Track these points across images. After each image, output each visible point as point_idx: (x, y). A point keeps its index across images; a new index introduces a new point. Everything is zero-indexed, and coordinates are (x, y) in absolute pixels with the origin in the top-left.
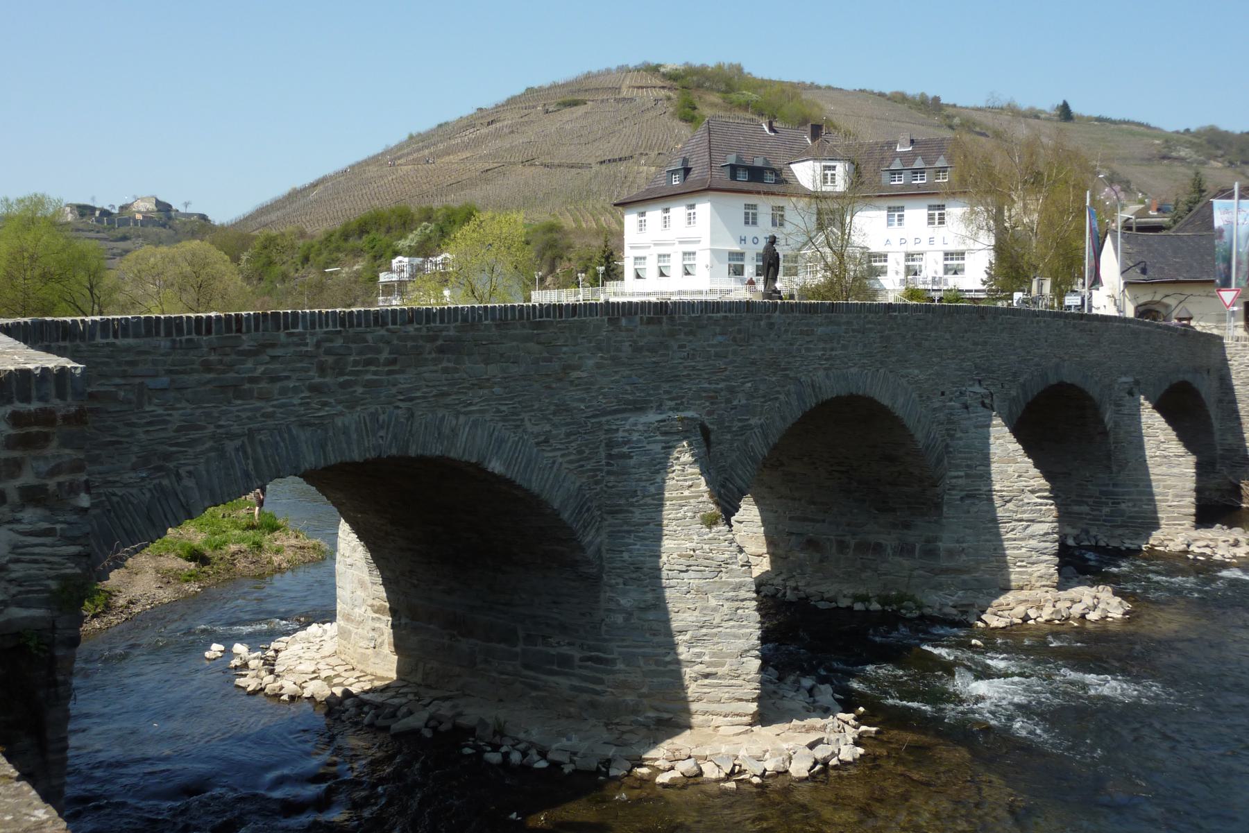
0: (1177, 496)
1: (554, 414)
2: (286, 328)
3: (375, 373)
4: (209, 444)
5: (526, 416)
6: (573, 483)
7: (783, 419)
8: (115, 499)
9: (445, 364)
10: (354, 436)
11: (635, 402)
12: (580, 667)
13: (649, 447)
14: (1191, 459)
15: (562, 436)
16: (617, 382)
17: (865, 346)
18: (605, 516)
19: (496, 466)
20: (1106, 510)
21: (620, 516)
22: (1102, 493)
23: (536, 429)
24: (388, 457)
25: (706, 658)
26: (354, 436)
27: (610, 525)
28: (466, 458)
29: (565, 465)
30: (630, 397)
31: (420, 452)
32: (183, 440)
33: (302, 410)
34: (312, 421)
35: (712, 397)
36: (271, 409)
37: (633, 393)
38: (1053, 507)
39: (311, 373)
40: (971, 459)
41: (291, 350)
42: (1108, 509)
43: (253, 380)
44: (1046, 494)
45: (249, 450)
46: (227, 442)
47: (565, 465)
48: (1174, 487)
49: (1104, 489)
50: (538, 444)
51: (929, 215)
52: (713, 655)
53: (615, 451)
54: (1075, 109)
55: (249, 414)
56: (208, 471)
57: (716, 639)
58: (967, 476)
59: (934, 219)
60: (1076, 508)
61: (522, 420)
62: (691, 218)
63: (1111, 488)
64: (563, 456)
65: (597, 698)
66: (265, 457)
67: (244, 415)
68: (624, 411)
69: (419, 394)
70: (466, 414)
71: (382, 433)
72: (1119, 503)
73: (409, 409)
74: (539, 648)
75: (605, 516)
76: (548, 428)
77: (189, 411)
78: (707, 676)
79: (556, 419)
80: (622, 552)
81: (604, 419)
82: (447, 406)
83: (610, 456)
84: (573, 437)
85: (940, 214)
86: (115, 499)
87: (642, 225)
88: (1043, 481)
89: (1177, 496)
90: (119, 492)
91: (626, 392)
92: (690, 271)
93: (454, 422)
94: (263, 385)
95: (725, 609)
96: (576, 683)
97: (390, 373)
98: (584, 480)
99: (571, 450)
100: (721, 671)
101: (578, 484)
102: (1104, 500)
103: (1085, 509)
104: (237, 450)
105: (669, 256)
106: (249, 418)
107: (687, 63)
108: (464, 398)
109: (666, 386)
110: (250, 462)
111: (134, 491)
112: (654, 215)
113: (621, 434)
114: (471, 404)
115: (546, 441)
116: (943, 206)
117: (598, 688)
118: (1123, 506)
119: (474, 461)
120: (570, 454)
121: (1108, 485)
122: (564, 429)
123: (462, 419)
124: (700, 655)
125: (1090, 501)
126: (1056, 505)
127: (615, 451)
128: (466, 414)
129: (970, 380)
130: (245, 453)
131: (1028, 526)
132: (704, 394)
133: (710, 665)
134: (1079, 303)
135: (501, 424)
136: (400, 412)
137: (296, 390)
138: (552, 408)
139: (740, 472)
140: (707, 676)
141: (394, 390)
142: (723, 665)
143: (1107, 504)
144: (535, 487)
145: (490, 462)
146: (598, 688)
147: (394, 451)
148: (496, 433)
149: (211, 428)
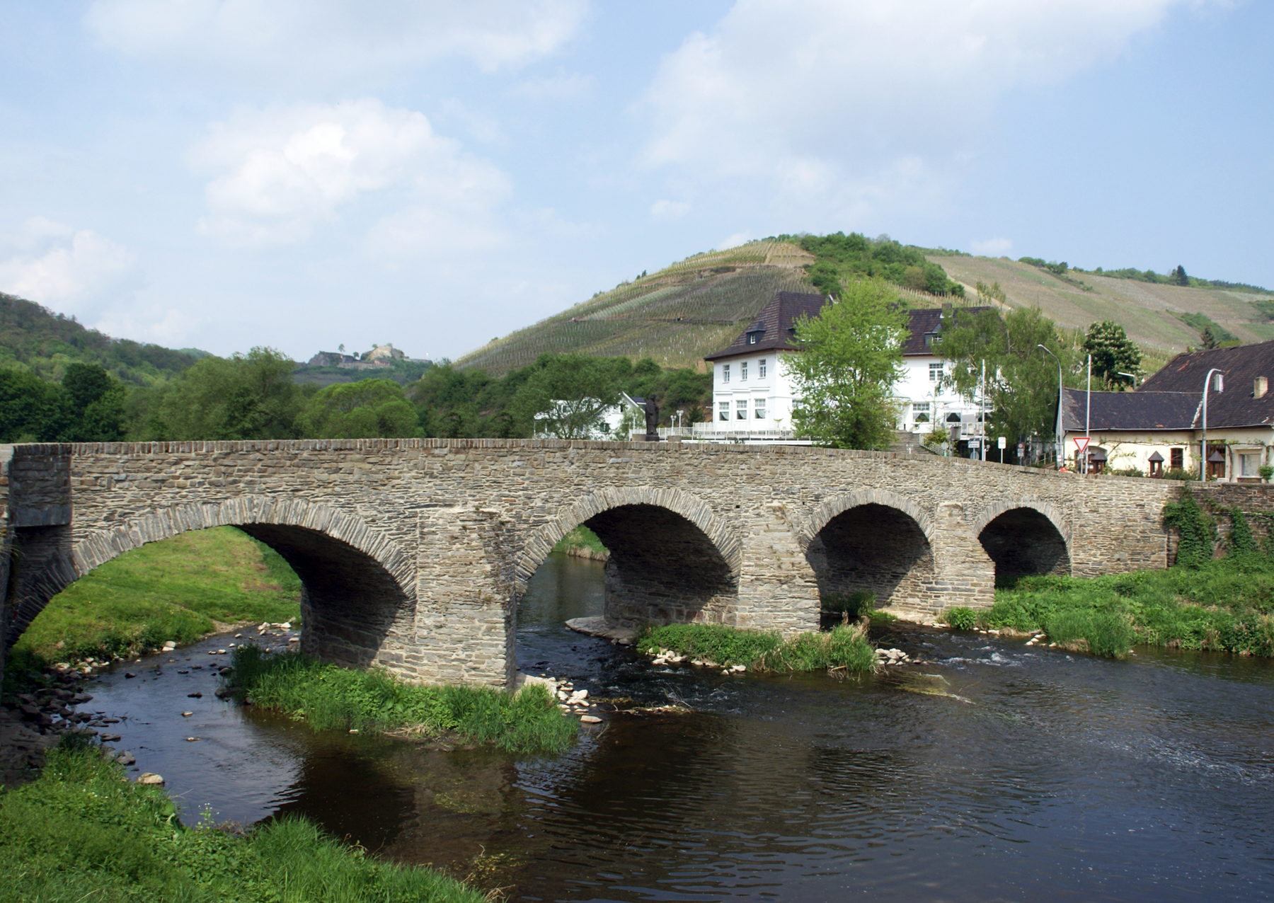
0: (981, 592)
1: (380, 505)
2: (196, 450)
3: (251, 476)
4: (149, 509)
5: (358, 506)
6: (395, 547)
7: (577, 517)
8: (94, 534)
9: (300, 473)
10: (238, 511)
11: (444, 501)
12: (406, 662)
13: (450, 528)
14: (992, 565)
15: (386, 518)
16: (431, 487)
17: (656, 472)
18: (418, 569)
19: (335, 534)
20: (930, 601)
21: (428, 570)
22: (928, 589)
23: (365, 514)
24: (260, 523)
25: (473, 659)
26: (238, 511)
27: (421, 575)
28: (313, 527)
29: (387, 536)
30: (440, 497)
31: (281, 522)
32: (133, 506)
33: (204, 495)
34: (210, 501)
35: (511, 501)
36: (185, 493)
37: (443, 495)
38: (816, 589)
39: (210, 475)
40: (759, 554)
41: (197, 462)
42: (932, 601)
43: (175, 478)
44: (813, 579)
45: (171, 514)
46: (158, 509)
47: (387, 536)
48: (979, 585)
49: (929, 586)
50: (367, 523)
51: (931, 372)
52: (477, 656)
53: (426, 530)
54: (1189, 272)
55: (172, 495)
56: (147, 524)
57: (479, 647)
58: (757, 565)
59: (934, 376)
60: (910, 600)
61: (355, 507)
62: (745, 373)
63: (934, 585)
64: (386, 530)
65: (413, 680)
66: (181, 518)
67: (169, 495)
68: (435, 506)
69: (281, 489)
70: (314, 502)
71: (256, 510)
72: (939, 597)
73: (274, 497)
74: (387, 650)
75: (418, 569)
76: (375, 513)
77: (136, 492)
78: (474, 669)
79: (381, 508)
80: (427, 592)
81: (418, 510)
82: (300, 497)
83: (422, 533)
84: (393, 520)
85: (939, 372)
86: (94, 534)
87: (727, 375)
88: (811, 570)
89: (981, 592)
90: (97, 531)
91: (436, 494)
92: (742, 415)
93: (305, 506)
94: (181, 480)
95: (484, 628)
96: (405, 672)
97: (261, 477)
98: (402, 546)
99: (392, 527)
100: (482, 667)
101: (397, 548)
102: (929, 594)
103: (917, 600)
104: (164, 514)
105: (746, 402)
106: (172, 498)
107: (884, 236)
108: (313, 492)
109: (472, 492)
110: (172, 521)
111: (104, 531)
112: (735, 366)
113: (431, 519)
114: (317, 497)
115: (373, 521)
116: (942, 365)
117: (414, 674)
118: (942, 599)
119: (319, 529)
120: (392, 530)
121: (931, 583)
122: (387, 515)
123: (311, 505)
124: (470, 656)
125: (920, 594)
126: (819, 587)
127: (426, 530)
128: (314, 502)
129: (767, 498)
130: (169, 515)
131: (798, 602)
132: (503, 498)
133: (476, 662)
134: (978, 446)
135: (339, 509)
136: (268, 498)
137: (201, 484)
138: (378, 501)
139: (536, 550)
140: (474, 669)
141: (264, 486)
142: (483, 663)
143: (931, 597)
144: (363, 548)
145: (330, 531)
146: (414, 674)
147: (264, 521)
148: (335, 514)
149: (149, 502)
